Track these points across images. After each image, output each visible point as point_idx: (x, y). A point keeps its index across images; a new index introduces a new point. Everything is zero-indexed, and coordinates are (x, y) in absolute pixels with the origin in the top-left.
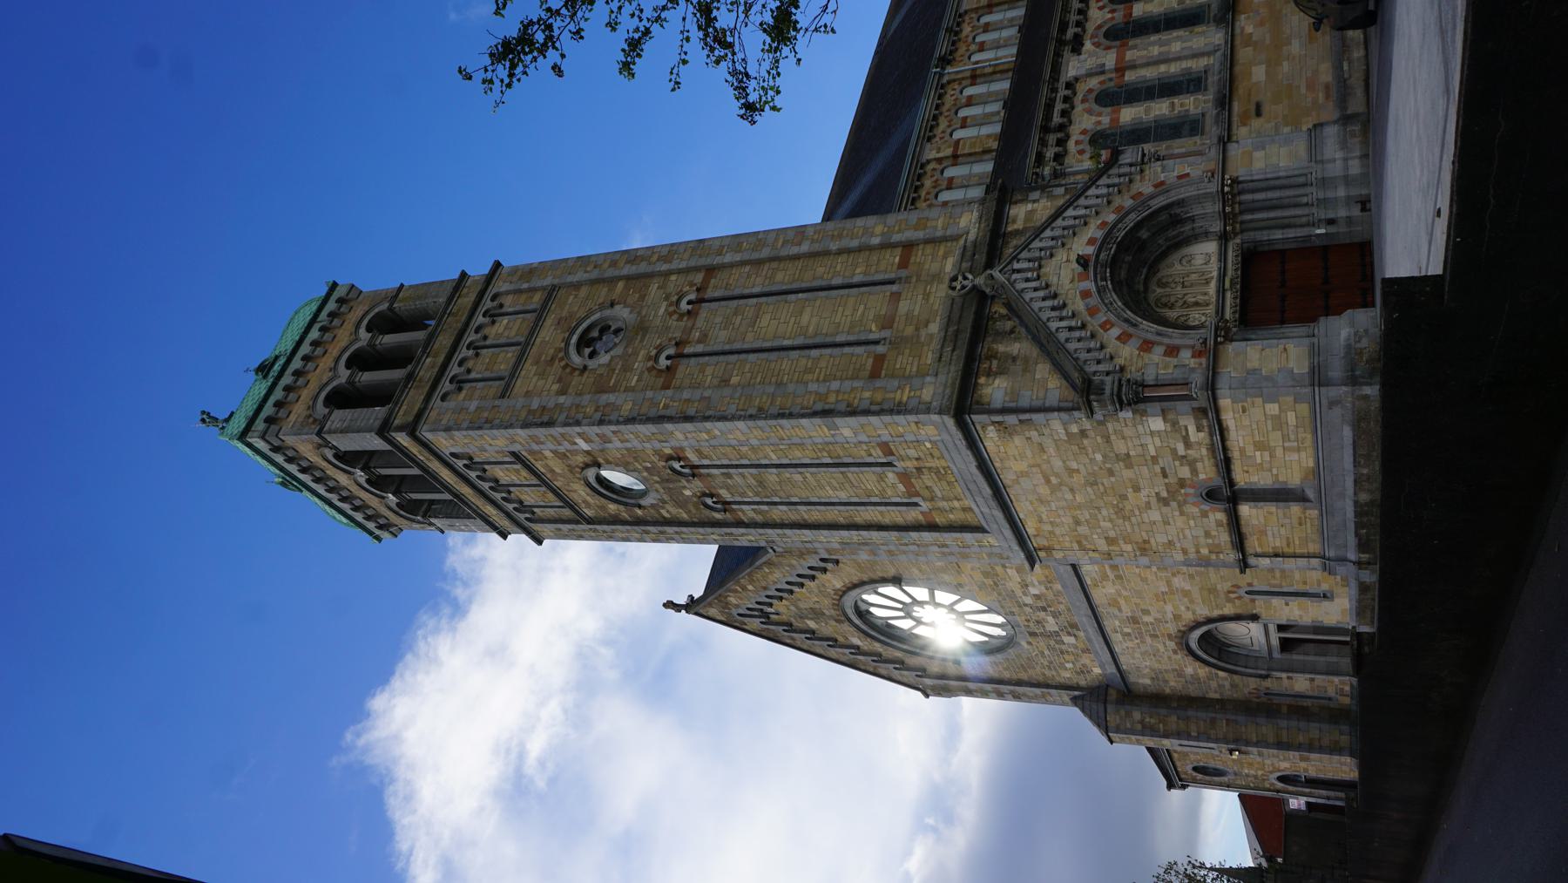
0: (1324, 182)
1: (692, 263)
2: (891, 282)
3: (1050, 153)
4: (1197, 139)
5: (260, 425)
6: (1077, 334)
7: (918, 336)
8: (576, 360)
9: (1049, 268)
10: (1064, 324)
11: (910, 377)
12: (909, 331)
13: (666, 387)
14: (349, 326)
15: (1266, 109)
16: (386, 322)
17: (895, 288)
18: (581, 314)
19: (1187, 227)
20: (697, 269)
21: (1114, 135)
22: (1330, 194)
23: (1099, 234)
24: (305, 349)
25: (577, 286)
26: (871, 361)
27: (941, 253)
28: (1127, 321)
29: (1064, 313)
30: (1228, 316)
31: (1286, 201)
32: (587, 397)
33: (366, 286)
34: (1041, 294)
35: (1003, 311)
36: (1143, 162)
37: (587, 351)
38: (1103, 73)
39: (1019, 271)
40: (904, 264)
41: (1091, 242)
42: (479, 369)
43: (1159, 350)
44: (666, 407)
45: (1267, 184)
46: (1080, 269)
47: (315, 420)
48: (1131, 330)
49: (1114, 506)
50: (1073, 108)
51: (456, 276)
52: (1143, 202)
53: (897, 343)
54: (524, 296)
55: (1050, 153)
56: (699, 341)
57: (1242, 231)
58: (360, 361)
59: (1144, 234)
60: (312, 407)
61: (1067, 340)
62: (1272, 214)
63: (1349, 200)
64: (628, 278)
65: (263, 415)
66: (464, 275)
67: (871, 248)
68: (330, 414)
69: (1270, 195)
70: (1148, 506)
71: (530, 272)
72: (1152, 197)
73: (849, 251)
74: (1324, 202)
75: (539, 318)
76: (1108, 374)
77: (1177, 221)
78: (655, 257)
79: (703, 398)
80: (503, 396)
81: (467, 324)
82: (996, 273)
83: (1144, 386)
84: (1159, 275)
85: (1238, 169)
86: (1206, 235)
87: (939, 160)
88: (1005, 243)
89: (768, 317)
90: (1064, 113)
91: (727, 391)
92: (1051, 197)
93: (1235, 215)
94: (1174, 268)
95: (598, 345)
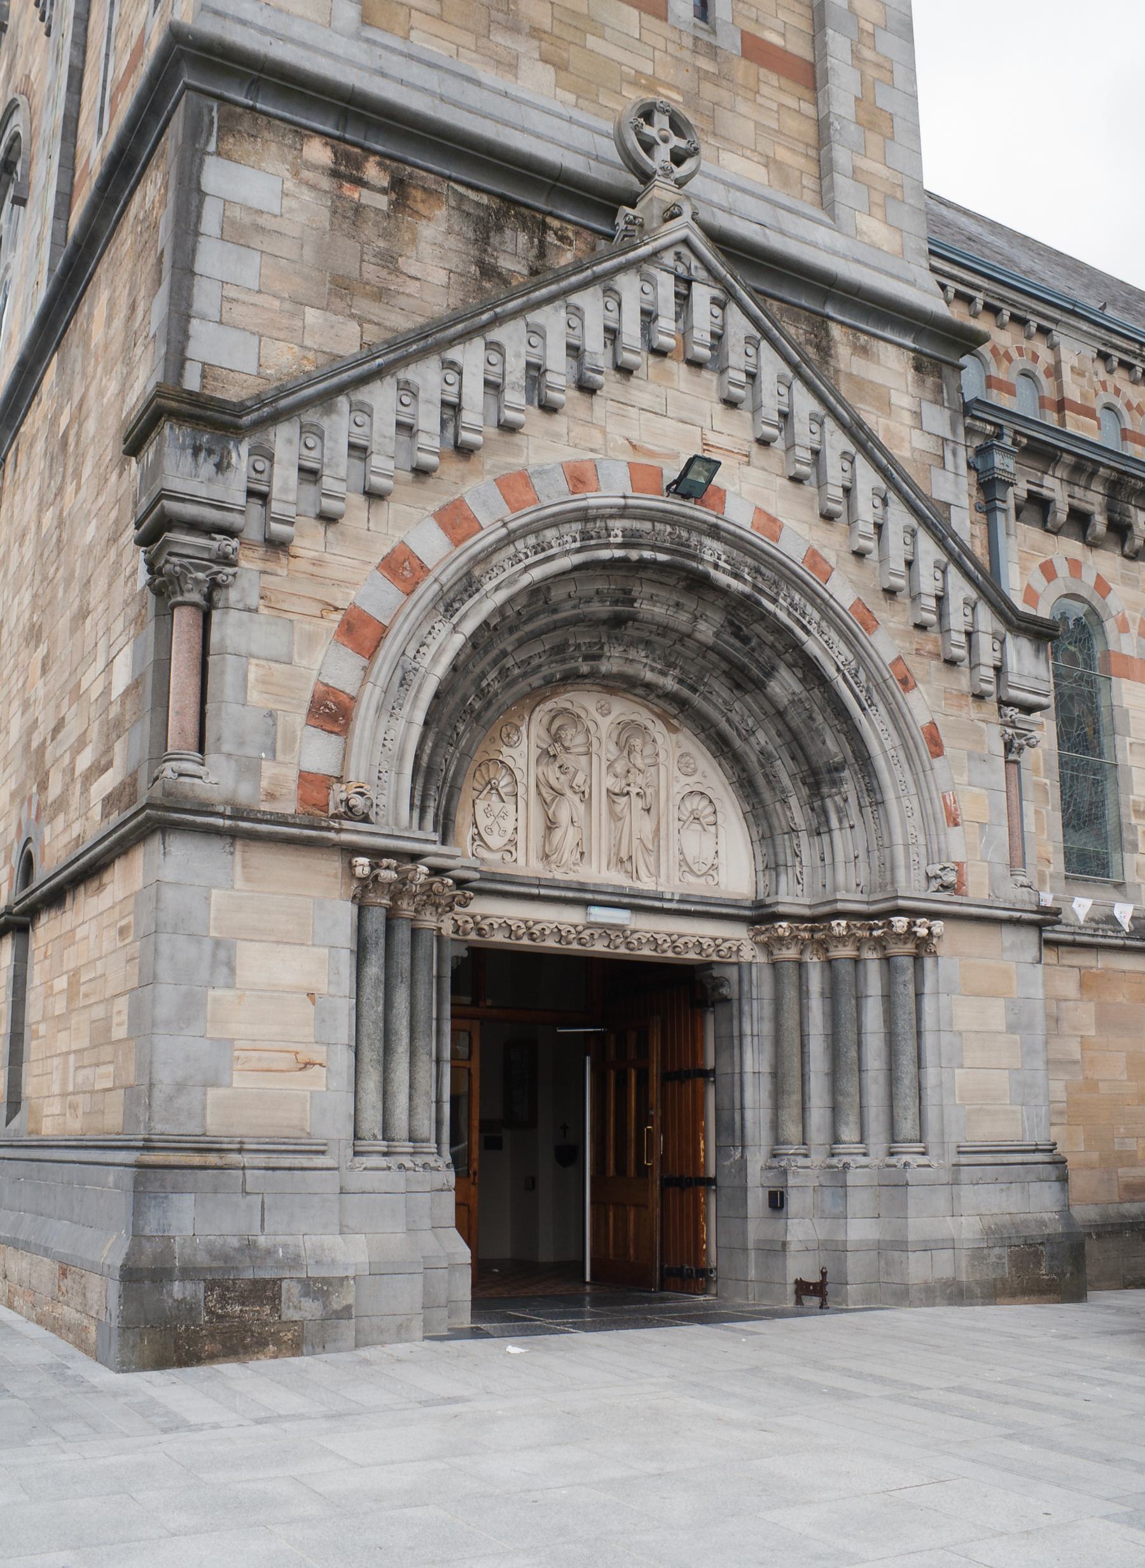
0: (894, 1186)
4: (1058, 865)
6: (429, 420)
7: (514, 29)
9: (694, 394)
19: (798, 814)
21: (1089, 662)
22: (859, 1200)
27: (783, 154)
28: (468, 585)
29: (515, 397)
30: (482, 907)
34: (594, 343)
36: (1003, 703)
39: (683, 299)
40: (755, 50)
43: (341, 669)
45: (905, 1037)
46: (672, 473)
48: (427, 590)
55: (1054, 487)
57: (774, 965)
59: (784, 685)
62: (817, 1046)
63: (837, 1250)
72: (896, 716)
74: (837, 1178)
77: (817, 780)
84: (658, 729)
85: (959, 955)
86: (773, 867)
87: (1055, 371)
93: (822, 946)
94: (679, 765)
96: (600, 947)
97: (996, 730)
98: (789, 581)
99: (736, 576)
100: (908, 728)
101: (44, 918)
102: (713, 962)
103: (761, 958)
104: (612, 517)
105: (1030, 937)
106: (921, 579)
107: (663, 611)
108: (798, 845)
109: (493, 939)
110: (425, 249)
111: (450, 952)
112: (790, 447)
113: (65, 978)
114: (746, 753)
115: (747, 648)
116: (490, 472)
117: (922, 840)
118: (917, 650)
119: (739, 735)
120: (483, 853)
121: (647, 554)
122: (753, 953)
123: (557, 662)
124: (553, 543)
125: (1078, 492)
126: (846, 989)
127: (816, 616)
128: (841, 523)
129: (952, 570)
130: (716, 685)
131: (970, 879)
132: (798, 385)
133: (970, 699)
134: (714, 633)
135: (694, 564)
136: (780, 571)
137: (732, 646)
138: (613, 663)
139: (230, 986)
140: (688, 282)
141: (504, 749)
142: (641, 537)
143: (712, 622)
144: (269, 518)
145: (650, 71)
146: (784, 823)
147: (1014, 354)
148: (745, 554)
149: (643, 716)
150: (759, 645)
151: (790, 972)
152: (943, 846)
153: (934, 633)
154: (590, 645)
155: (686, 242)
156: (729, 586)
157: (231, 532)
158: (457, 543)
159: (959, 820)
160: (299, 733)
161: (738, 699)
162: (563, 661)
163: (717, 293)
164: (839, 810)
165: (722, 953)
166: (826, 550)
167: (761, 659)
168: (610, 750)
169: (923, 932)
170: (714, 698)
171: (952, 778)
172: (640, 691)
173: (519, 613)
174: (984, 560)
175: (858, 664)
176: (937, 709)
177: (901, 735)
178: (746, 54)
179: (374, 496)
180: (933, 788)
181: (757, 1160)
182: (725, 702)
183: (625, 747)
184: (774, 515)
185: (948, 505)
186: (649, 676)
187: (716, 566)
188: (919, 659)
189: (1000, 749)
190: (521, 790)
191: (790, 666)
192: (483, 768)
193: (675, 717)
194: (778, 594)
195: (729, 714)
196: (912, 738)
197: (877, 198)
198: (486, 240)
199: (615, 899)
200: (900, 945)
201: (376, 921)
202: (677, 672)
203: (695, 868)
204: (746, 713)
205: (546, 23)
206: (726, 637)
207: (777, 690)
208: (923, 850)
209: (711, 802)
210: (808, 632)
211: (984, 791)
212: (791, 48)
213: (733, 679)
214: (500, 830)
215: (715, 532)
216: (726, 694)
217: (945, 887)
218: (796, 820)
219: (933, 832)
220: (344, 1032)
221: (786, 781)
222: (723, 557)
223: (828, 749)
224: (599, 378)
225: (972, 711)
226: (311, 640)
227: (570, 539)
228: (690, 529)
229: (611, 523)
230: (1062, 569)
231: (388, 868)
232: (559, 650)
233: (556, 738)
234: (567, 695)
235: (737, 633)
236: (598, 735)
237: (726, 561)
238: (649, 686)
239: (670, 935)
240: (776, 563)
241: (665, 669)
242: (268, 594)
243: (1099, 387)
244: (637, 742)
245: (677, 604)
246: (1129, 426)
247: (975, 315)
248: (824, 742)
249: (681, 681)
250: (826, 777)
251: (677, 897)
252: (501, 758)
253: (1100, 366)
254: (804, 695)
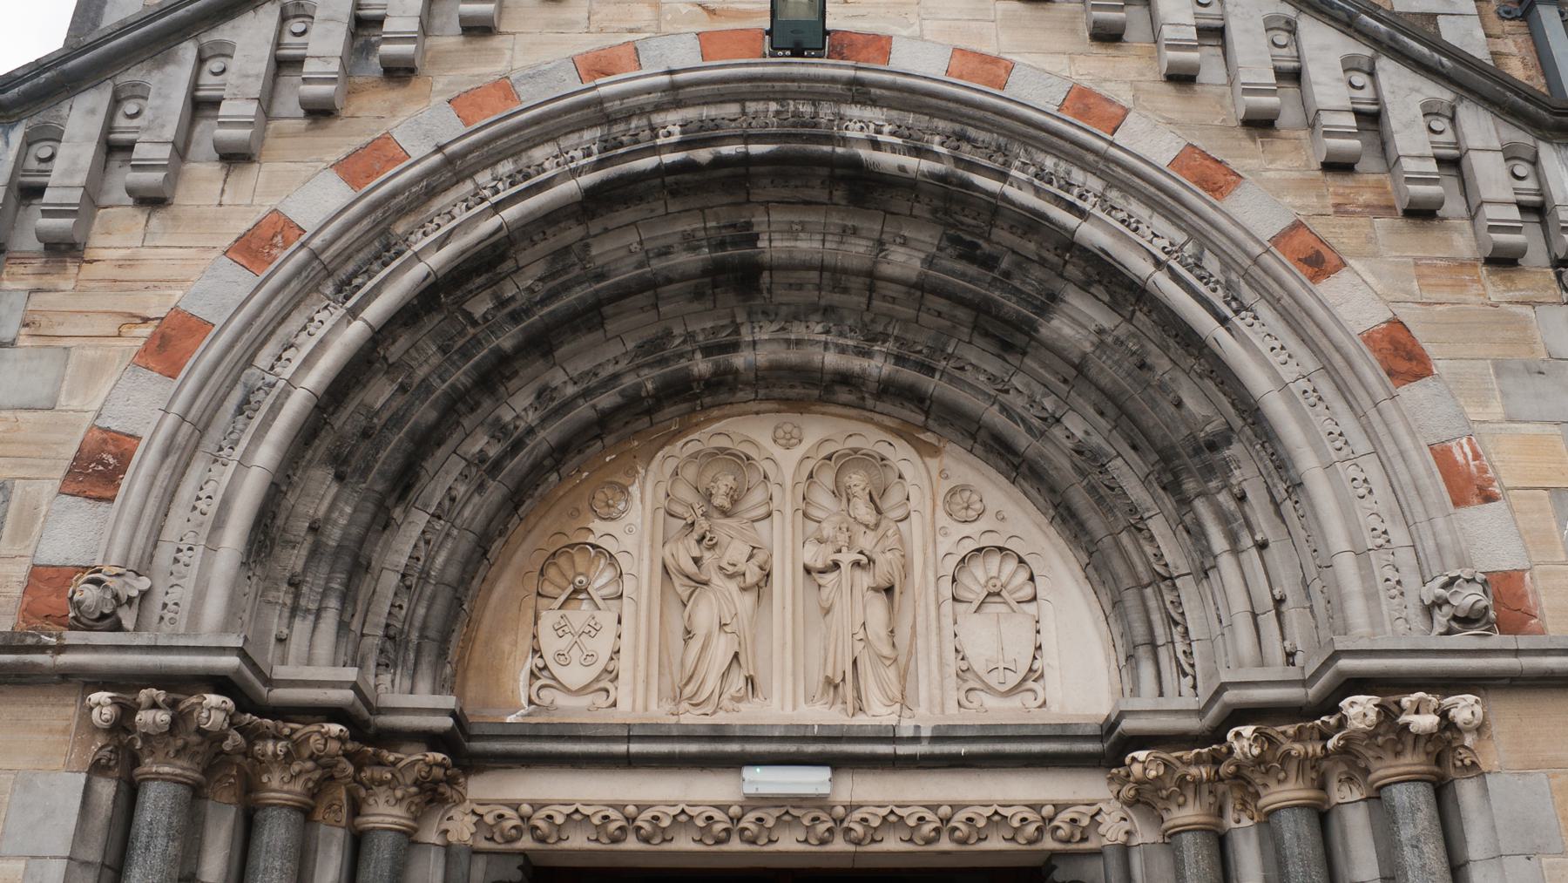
59: (1078, 321)
72: (1294, 319)
84: (900, 455)
94: (941, 505)
96: (788, 842)
98: (1027, 141)
99: (919, 152)
100: (1325, 334)
102: (1054, 854)
104: (659, 108)
106: (1316, 89)
107: (817, 245)
108: (1178, 603)
109: (565, 845)
114: (1042, 455)
115: (996, 274)
116: (441, 92)
117: (1399, 536)
118: (1336, 206)
119: (1030, 429)
121: (728, 150)
122: (1127, 826)
123: (650, 365)
124: (547, 165)
127: (1096, 184)
130: (972, 355)
131: (1544, 601)
133: (1483, 271)
134: (924, 261)
135: (827, 148)
136: (1002, 127)
137: (963, 276)
138: (761, 348)
141: (598, 525)
142: (718, 127)
143: (919, 246)
146: (1140, 568)
148: (932, 116)
149: (870, 439)
150: (1019, 265)
152: (1446, 539)
153: (1369, 164)
154: (715, 331)
156: (902, 169)
159: (1496, 489)
160: (44, 509)
161: (1019, 369)
162: (663, 362)
164: (1224, 519)
165: (1061, 833)
166: (1108, 86)
167: (1027, 289)
170: (969, 376)
171: (1462, 414)
172: (844, 395)
173: (530, 290)
174: (1539, 84)
175: (1201, 247)
176: (1402, 296)
177: (1316, 351)
180: (1401, 430)
182: (992, 379)
184: (995, 54)
185: (1432, 17)
186: (832, 360)
188: (1345, 220)
191: (1085, 287)
193: (926, 429)
194: (1006, 164)
195: (1002, 397)
196: (1338, 349)
199: (791, 748)
200: (1389, 760)
202: (890, 345)
203: (993, 680)
204: (1038, 390)
206: (948, 264)
207: (1067, 331)
208: (1406, 557)
209: (1021, 561)
210: (1082, 214)
211: (1550, 428)
213: (994, 336)
215: (859, 92)
216: (993, 366)
217: (1466, 620)
218: (1168, 558)
219: (1420, 516)
221: (1136, 492)
222: (887, 129)
223: (1191, 414)
226: (94, 370)
227: (578, 154)
228: (815, 98)
229: (658, 119)
231: (154, 705)
232: (653, 349)
234: (716, 427)
235: (969, 253)
236: (976, 536)
237: (893, 134)
238: (845, 379)
239: (933, 808)
240: (989, 115)
241: (865, 345)
242: (37, 318)
245: (844, 230)
248: (1179, 404)
249: (900, 360)
250: (1194, 464)
251: (926, 732)
252: (591, 539)
254: (1124, 330)
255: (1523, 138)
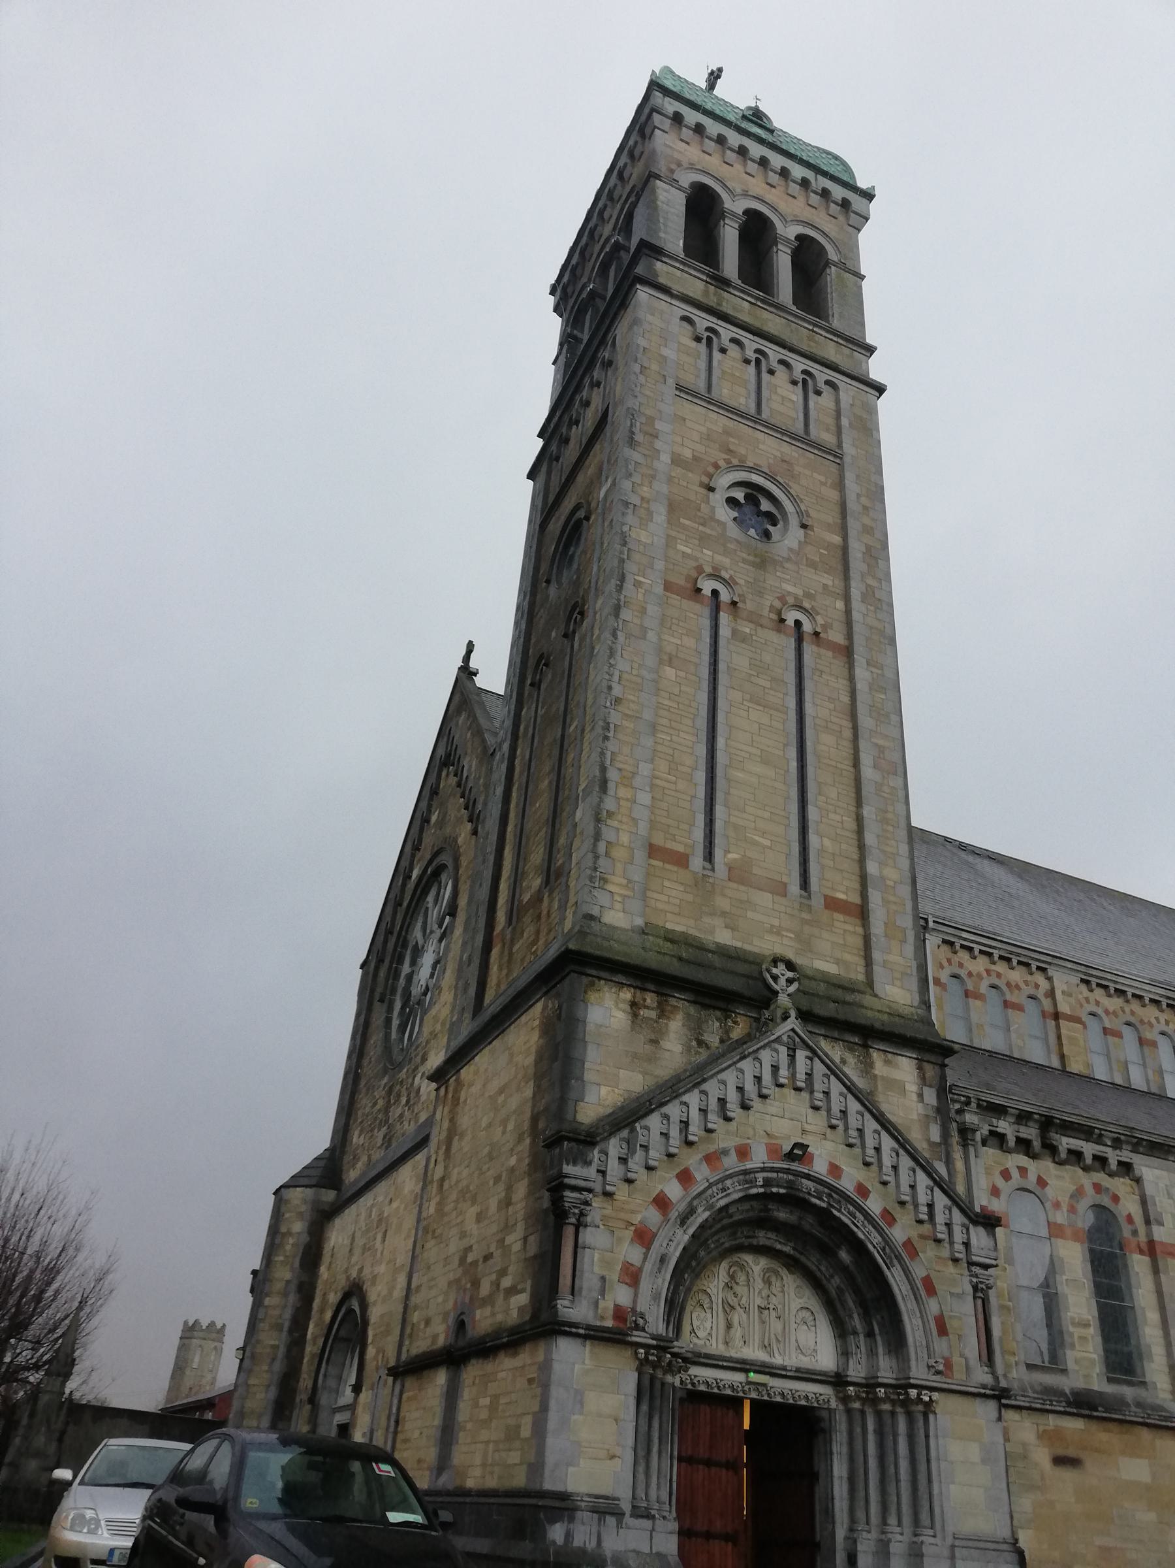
1: (857, 628)
2: (805, 884)
3: (1004, 1126)
5: (671, 106)
6: (674, 1132)
7: (712, 914)
8: (724, 481)
9: (797, 1104)
10: (694, 1114)
11: (644, 899)
12: (722, 903)
13: (668, 586)
14: (808, 214)
15: (1067, 1475)
16: (810, 260)
17: (795, 888)
18: (795, 489)
19: (857, 1322)
20: (850, 635)
23: (847, 1184)
24: (777, 161)
25: (840, 485)
26: (680, 848)
27: (847, 957)
28: (691, 1211)
29: (712, 1117)
30: (695, 1371)
31: (892, 1489)
32: (665, 489)
33: (866, 238)
34: (750, 1087)
35: (737, 1033)
36: (971, 1264)
37: (739, 495)
38: (1148, 1222)
39: (792, 1057)
40: (832, 904)
41: (835, 1170)
42: (729, 363)
43: (634, 1254)
44: (637, 584)
46: (787, 1148)
47: (672, 171)
48: (673, 1215)
49: (468, 1187)
50: (1086, 1169)
51: (870, 340)
52: (899, 1258)
53: (703, 886)
54: (831, 421)
55: (1004, 1126)
56: (734, 632)
57: (849, 1411)
58: (756, 229)
60: (692, 168)
61: (666, 1117)
62: (873, 1463)
64: (845, 549)
65: (685, 110)
66: (870, 350)
67: (862, 861)
68: (680, 189)
69: (904, 1465)
70: (463, 1235)
71: (868, 428)
72: (907, 1272)
73: (860, 831)
75: (794, 437)
76: (603, 1173)
78: (870, 581)
79: (644, 630)
80: (680, 388)
81: (792, 350)
82: (792, 1023)
83: (577, 1227)
84: (784, 1272)
86: (844, 1353)
87: (1051, 994)
88: (851, 1047)
89: (765, 720)
90: (1076, 1156)
91: (651, 661)
92: (926, 1120)
94: (794, 1297)
95: (748, 509)
97: (966, 1279)
99: (820, 1199)
101: (473, 1361)
103: (841, 1407)
105: (992, 1405)
110: (672, 1035)
111: (679, 1394)
112: (846, 1129)
113: (488, 1399)
120: (695, 1340)
121: (774, 1190)
125: (1022, 1129)
126: (888, 1429)
127: (862, 1218)
128: (874, 1168)
129: (936, 1189)
132: (849, 1096)
139: (581, 1413)
140: (794, 1051)
144: (605, 1183)
145: (777, 924)
147: (1022, 985)
151: (857, 1416)
155: (793, 1030)
157: (590, 1191)
158: (685, 1189)
163: (808, 1053)
168: (759, 1284)
169: (927, 1399)
178: (827, 906)
179: (649, 1168)
181: (841, 1533)
183: (768, 1282)
187: (809, 1194)
189: (970, 1289)
190: (714, 1306)
192: (649, 894)
197: (897, 975)
198: (699, 1027)
201: (646, 1382)
205: (727, 908)
212: (850, 900)
214: (704, 1330)
220: (630, 1441)
224: (751, 1103)
225: (951, 1269)
229: (757, 1175)
230: (1015, 1174)
233: (732, 1277)
238: (779, 1251)
243: (1083, 1002)
244: (773, 1279)
246: (1107, 1025)
247: (994, 963)
249: (794, 1249)
253: (1083, 987)
255: (967, 1222)
